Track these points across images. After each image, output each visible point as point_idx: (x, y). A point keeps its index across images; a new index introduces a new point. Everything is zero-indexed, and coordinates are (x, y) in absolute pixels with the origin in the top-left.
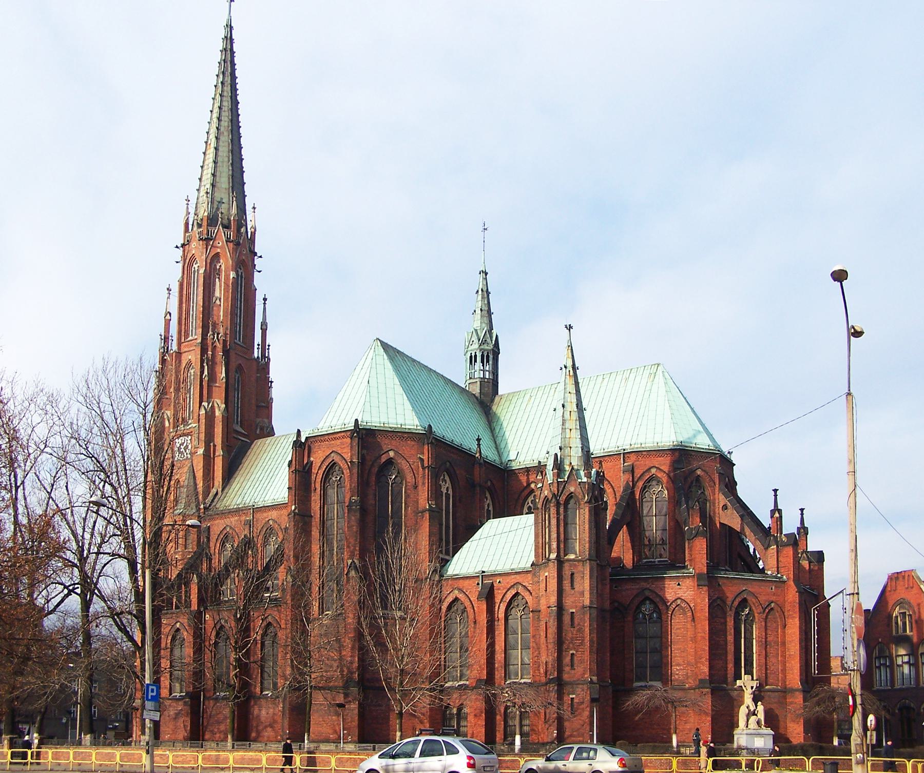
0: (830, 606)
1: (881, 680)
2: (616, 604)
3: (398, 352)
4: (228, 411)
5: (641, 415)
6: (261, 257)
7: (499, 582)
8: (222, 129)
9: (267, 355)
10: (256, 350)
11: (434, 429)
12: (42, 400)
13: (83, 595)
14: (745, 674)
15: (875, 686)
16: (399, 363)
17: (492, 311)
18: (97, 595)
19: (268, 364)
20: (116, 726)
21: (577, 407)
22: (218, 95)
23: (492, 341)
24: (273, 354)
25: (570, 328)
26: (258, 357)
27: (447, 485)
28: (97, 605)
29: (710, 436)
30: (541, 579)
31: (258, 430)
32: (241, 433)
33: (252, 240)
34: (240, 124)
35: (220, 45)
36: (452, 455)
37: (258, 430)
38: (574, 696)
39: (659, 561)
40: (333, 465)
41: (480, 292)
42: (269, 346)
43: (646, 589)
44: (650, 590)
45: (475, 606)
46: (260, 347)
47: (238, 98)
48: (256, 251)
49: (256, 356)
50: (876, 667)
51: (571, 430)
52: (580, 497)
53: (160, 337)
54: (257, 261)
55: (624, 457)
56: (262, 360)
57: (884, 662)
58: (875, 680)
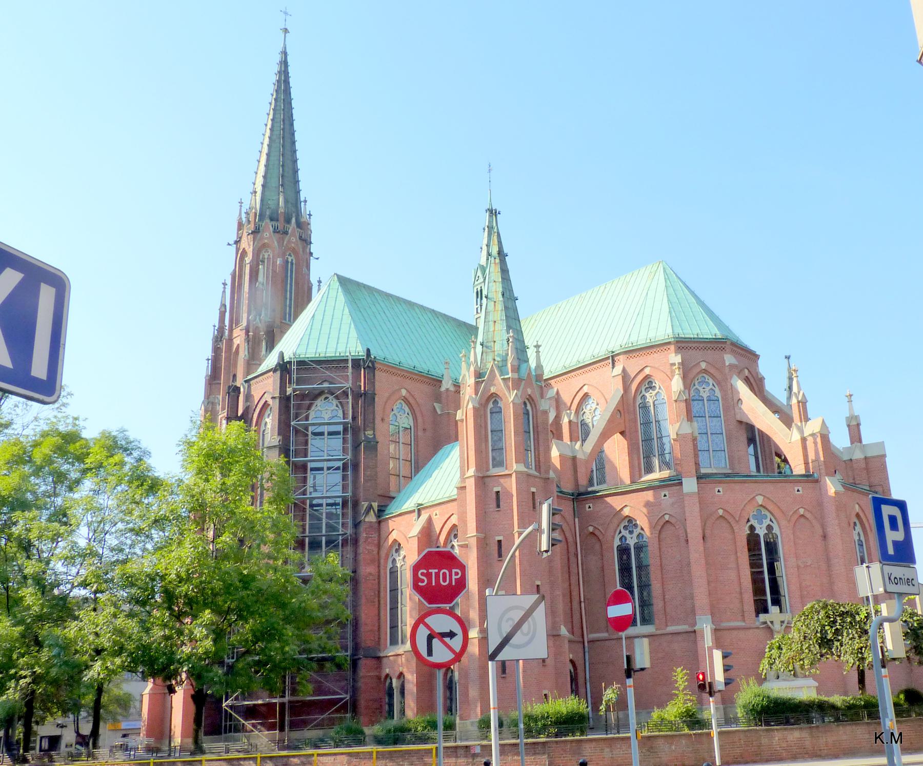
11: (373, 354)
21: (503, 295)
22: (272, 110)
25: (788, 358)
35: (276, 68)
41: (486, 229)
51: (495, 322)
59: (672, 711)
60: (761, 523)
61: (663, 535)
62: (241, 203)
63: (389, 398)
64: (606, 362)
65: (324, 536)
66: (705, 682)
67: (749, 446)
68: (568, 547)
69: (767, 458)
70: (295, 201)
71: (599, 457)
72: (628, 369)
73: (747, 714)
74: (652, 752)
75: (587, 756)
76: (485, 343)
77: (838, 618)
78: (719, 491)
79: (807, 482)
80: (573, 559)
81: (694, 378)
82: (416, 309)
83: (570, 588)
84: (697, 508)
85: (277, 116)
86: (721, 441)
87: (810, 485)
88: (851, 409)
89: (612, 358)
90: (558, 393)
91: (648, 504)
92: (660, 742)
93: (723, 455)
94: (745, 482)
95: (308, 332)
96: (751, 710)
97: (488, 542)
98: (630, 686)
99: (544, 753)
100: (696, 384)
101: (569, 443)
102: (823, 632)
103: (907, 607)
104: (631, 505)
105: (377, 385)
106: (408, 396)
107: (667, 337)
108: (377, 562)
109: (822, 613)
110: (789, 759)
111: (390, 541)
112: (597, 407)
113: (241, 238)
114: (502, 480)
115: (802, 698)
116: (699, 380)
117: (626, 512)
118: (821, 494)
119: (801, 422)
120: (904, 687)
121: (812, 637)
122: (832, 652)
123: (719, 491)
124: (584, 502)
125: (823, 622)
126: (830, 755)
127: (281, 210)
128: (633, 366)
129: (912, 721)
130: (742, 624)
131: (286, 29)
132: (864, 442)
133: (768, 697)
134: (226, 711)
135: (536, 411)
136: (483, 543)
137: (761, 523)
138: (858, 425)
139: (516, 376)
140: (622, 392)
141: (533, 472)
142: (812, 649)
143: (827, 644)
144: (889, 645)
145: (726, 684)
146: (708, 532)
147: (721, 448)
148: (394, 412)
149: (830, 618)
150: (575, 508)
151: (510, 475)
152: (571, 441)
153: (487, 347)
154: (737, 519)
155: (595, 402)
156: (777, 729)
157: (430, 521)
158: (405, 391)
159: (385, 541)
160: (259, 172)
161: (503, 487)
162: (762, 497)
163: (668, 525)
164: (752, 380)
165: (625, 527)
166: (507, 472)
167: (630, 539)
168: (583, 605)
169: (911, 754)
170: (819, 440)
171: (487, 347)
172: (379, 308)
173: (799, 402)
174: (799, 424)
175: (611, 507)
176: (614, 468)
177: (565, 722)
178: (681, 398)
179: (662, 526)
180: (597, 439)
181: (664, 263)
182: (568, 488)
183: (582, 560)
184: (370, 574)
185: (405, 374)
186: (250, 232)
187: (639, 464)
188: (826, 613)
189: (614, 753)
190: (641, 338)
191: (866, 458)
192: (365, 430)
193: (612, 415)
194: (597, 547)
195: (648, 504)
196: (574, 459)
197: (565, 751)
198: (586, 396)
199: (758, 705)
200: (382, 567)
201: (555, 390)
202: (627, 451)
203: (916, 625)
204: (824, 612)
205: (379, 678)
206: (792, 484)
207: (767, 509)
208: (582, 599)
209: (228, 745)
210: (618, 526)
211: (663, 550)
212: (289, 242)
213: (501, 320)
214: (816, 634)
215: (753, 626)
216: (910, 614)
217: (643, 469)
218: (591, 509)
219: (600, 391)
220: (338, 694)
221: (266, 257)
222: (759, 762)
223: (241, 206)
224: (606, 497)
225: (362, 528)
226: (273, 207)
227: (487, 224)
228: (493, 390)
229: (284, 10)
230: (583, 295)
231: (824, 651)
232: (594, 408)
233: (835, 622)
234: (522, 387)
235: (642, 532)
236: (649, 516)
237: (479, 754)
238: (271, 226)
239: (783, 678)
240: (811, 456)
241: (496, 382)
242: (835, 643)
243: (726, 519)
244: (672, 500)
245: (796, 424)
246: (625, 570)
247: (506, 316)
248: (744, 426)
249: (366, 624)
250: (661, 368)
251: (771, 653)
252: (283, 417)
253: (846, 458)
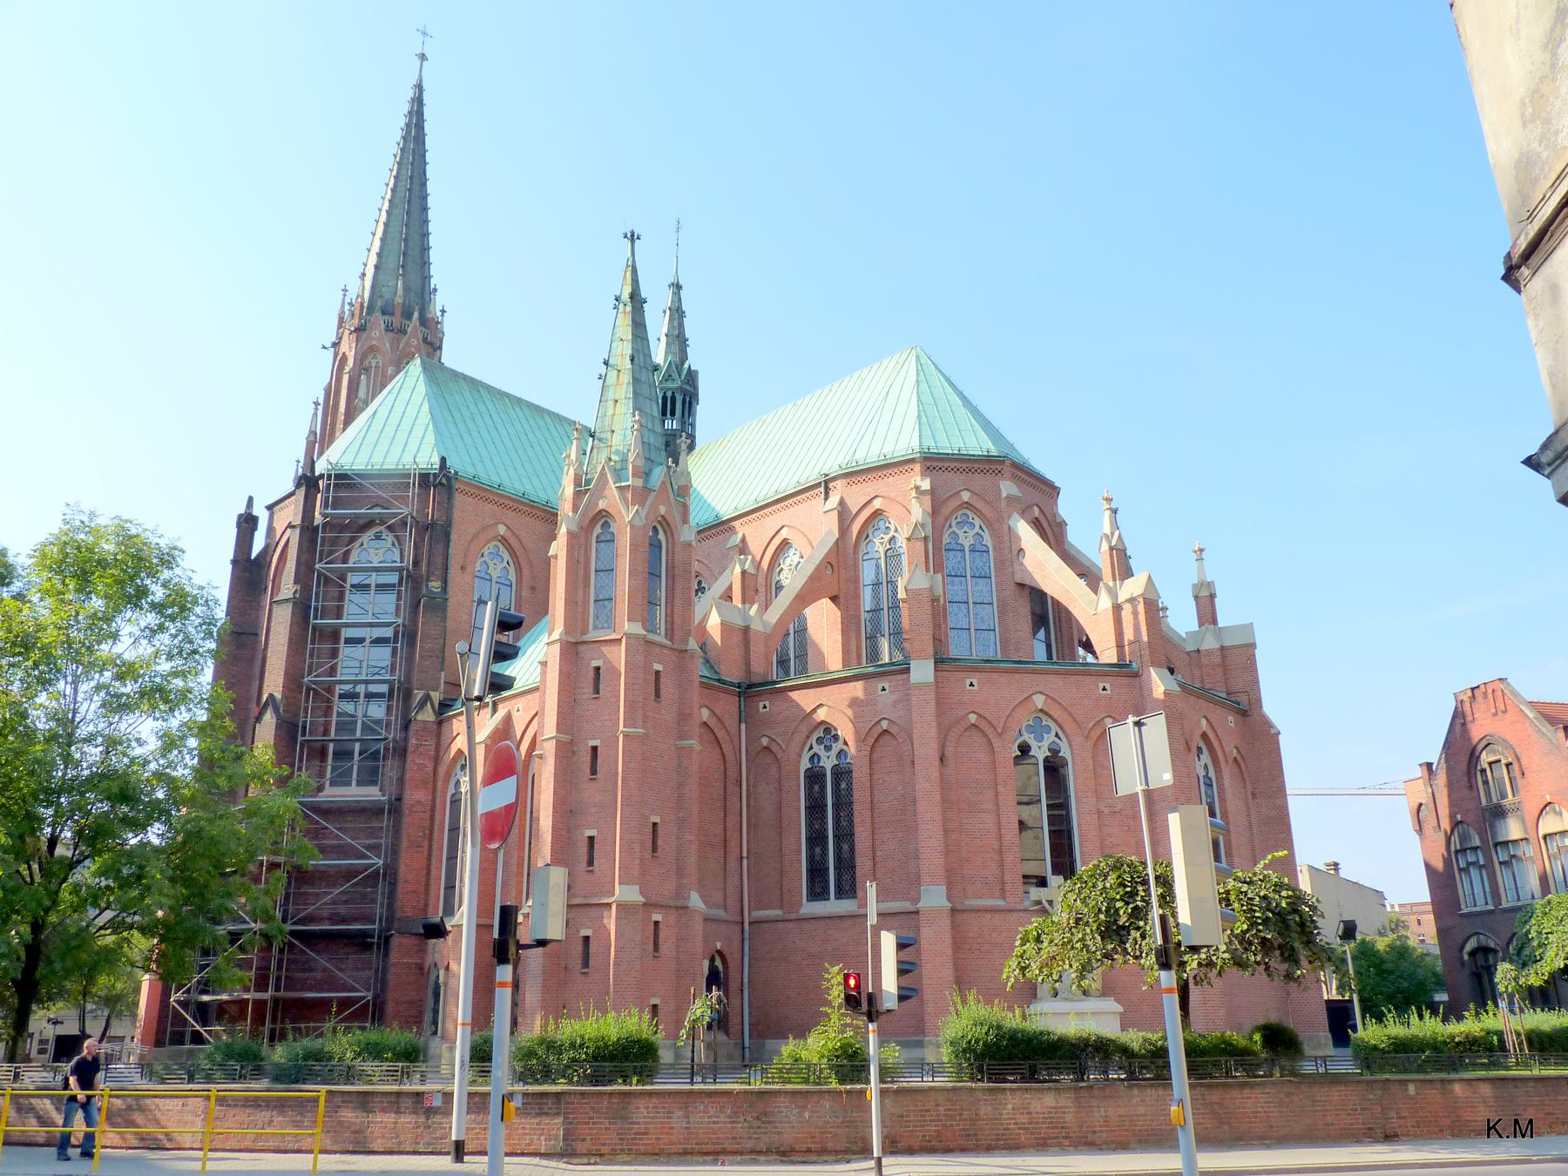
23: (680, 376)
29: (986, 425)
41: (668, 312)
50: (1460, 870)
59: (816, 1046)
60: (1040, 739)
61: (875, 756)
62: (345, 290)
63: (475, 537)
64: (816, 491)
65: (357, 740)
66: (859, 993)
67: (1035, 632)
68: (725, 769)
69: (1065, 645)
70: (421, 292)
71: (795, 633)
72: (849, 502)
73: (957, 1056)
74: (764, 1123)
75: (639, 1123)
76: (597, 434)
77: (1140, 888)
78: (971, 685)
79: (1118, 675)
80: (732, 788)
81: (951, 514)
82: (546, 417)
83: (725, 834)
84: (931, 709)
85: (402, 172)
86: (990, 616)
87: (1125, 681)
88: (1201, 571)
89: (826, 484)
90: (743, 540)
91: (854, 703)
92: (783, 1102)
93: (992, 636)
94: (1016, 671)
95: (362, 435)
96: (964, 1051)
97: (575, 749)
98: (503, 985)
99: (558, 1114)
100: (953, 524)
101: (740, 606)
102: (1112, 912)
103: (1270, 872)
104: (830, 704)
105: (457, 515)
106: (508, 535)
107: (910, 452)
108: (432, 783)
109: (1112, 878)
110: (1031, 1146)
111: (453, 752)
112: (801, 560)
113: (341, 338)
114: (605, 649)
115: (1064, 1031)
116: (959, 519)
117: (821, 715)
118: (1142, 695)
119: (1114, 580)
120: (1261, 1021)
121: (1091, 920)
122: (1126, 949)
123: (971, 685)
124: (757, 699)
125: (1112, 894)
126: (1113, 1142)
127: (399, 300)
128: (856, 496)
129: (1273, 1083)
130: (1000, 903)
131: (424, 55)
132: (1221, 624)
133: (999, 1027)
134: (173, 1006)
135: (673, 544)
136: (566, 751)
137: (1040, 739)
138: (1212, 596)
139: (640, 483)
140: (837, 536)
141: (661, 638)
142: (1089, 943)
143: (1118, 934)
144: (1184, 915)
145: (902, 998)
146: (950, 751)
147: (989, 625)
148: (483, 559)
149: (1125, 886)
150: (742, 706)
151: (620, 640)
152: (744, 602)
153: (600, 440)
154: (1000, 731)
155: (798, 553)
156: (1010, 1089)
157: (508, 720)
158: (505, 528)
159: (446, 751)
160: (373, 249)
161: (606, 660)
162: (1044, 697)
163: (887, 737)
164: (1045, 525)
165: (820, 741)
166: (614, 636)
167: (826, 759)
168: (745, 862)
169: (1268, 1147)
170: (1141, 608)
171: (600, 440)
172: (484, 410)
173: (1111, 549)
174: (1111, 583)
175: (798, 706)
176: (820, 654)
177: (612, 1058)
178: (917, 535)
179: (877, 738)
180: (788, 603)
181: (919, 350)
182: (733, 674)
183: (748, 790)
184: (420, 802)
185: (507, 502)
186: (353, 329)
187: (859, 647)
188: (1119, 877)
189: (692, 1119)
190: (870, 454)
191: (1223, 649)
192: (428, 580)
193: (817, 569)
194: (774, 770)
195: (854, 703)
196: (746, 630)
197: (597, 1112)
198: (785, 544)
199: (977, 1041)
200: (439, 793)
201: (740, 536)
202: (840, 627)
203: (1284, 905)
204: (1114, 876)
205: (420, 967)
206: (1094, 678)
207: (1050, 716)
208: (745, 854)
209: (20, 1068)
210: (808, 737)
211: (875, 777)
212: (408, 344)
213: (626, 398)
214: (1096, 915)
215: (1018, 907)
216: (1276, 885)
217: (864, 656)
218: (767, 709)
219: (805, 536)
220: (353, 989)
221: (373, 364)
222: (973, 1150)
223: (345, 295)
224: (791, 691)
225: (413, 727)
226: (387, 296)
227: (669, 304)
228: (602, 505)
229: (421, 28)
230: (798, 403)
231: (1110, 947)
232: (795, 563)
233: (1133, 894)
234: (648, 503)
235: (845, 748)
236: (856, 722)
237: (440, 1108)
238: (382, 322)
239: (1064, 996)
240: (1129, 635)
241: (607, 492)
242: (1133, 932)
243: (982, 731)
244: (896, 696)
245: (1105, 584)
246: (815, 808)
247: (634, 392)
248: (1026, 592)
249: (407, 882)
250: (899, 499)
251: (1024, 948)
252: (304, 557)
253: (1190, 647)
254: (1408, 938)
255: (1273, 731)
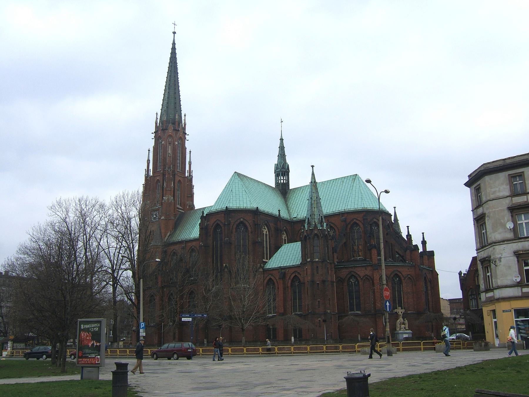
0: (438, 275)
1: (473, 305)
2: (339, 278)
3: (245, 176)
4: (174, 200)
5: (349, 196)
6: (188, 135)
7: (288, 271)
8: (171, 85)
9: (191, 175)
10: (186, 173)
12: (97, 207)
13: (113, 285)
14: (398, 307)
15: (479, 307)
16: (245, 181)
17: (286, 155)
18: (119, 285)
19: (192, 179)
20: (124, 339)
24: (194, 174)
26: (187, 176)
27: (266, 230)
28: (119, 288)
30: (305, 269)
31: (188, 206)
32: (180, 208)
33: (184, 129)
34: (179, 82)
36: (268, 218)
37: (188, 206)
38: (320, 319)
39: (359, 258)
40: (218, 225)
42: (192, 171)
43: (352, 271)
44: (354, 272)
45: (278, 281)
46: (188, 172)
47: (178, 71)
48: (186, 132)
49: (186, 175)
50: (470, 299)
51: (314, 208)
52: (319, 235)
53: (145, 170)
54: (187, 136)
55: (342, 215)
56: (189, 177)
57: (474, 297)
58: (470, 305)
62: (157, 114)
132: (476, 256)
254: (498, 344)
255: (185, 148)
